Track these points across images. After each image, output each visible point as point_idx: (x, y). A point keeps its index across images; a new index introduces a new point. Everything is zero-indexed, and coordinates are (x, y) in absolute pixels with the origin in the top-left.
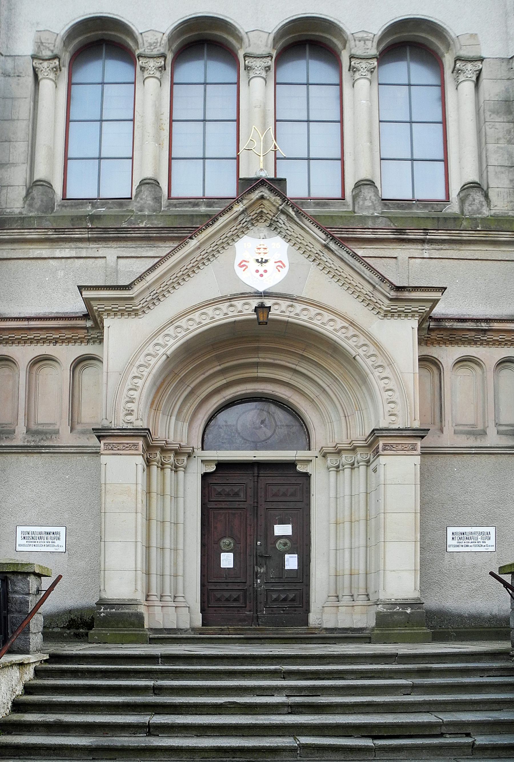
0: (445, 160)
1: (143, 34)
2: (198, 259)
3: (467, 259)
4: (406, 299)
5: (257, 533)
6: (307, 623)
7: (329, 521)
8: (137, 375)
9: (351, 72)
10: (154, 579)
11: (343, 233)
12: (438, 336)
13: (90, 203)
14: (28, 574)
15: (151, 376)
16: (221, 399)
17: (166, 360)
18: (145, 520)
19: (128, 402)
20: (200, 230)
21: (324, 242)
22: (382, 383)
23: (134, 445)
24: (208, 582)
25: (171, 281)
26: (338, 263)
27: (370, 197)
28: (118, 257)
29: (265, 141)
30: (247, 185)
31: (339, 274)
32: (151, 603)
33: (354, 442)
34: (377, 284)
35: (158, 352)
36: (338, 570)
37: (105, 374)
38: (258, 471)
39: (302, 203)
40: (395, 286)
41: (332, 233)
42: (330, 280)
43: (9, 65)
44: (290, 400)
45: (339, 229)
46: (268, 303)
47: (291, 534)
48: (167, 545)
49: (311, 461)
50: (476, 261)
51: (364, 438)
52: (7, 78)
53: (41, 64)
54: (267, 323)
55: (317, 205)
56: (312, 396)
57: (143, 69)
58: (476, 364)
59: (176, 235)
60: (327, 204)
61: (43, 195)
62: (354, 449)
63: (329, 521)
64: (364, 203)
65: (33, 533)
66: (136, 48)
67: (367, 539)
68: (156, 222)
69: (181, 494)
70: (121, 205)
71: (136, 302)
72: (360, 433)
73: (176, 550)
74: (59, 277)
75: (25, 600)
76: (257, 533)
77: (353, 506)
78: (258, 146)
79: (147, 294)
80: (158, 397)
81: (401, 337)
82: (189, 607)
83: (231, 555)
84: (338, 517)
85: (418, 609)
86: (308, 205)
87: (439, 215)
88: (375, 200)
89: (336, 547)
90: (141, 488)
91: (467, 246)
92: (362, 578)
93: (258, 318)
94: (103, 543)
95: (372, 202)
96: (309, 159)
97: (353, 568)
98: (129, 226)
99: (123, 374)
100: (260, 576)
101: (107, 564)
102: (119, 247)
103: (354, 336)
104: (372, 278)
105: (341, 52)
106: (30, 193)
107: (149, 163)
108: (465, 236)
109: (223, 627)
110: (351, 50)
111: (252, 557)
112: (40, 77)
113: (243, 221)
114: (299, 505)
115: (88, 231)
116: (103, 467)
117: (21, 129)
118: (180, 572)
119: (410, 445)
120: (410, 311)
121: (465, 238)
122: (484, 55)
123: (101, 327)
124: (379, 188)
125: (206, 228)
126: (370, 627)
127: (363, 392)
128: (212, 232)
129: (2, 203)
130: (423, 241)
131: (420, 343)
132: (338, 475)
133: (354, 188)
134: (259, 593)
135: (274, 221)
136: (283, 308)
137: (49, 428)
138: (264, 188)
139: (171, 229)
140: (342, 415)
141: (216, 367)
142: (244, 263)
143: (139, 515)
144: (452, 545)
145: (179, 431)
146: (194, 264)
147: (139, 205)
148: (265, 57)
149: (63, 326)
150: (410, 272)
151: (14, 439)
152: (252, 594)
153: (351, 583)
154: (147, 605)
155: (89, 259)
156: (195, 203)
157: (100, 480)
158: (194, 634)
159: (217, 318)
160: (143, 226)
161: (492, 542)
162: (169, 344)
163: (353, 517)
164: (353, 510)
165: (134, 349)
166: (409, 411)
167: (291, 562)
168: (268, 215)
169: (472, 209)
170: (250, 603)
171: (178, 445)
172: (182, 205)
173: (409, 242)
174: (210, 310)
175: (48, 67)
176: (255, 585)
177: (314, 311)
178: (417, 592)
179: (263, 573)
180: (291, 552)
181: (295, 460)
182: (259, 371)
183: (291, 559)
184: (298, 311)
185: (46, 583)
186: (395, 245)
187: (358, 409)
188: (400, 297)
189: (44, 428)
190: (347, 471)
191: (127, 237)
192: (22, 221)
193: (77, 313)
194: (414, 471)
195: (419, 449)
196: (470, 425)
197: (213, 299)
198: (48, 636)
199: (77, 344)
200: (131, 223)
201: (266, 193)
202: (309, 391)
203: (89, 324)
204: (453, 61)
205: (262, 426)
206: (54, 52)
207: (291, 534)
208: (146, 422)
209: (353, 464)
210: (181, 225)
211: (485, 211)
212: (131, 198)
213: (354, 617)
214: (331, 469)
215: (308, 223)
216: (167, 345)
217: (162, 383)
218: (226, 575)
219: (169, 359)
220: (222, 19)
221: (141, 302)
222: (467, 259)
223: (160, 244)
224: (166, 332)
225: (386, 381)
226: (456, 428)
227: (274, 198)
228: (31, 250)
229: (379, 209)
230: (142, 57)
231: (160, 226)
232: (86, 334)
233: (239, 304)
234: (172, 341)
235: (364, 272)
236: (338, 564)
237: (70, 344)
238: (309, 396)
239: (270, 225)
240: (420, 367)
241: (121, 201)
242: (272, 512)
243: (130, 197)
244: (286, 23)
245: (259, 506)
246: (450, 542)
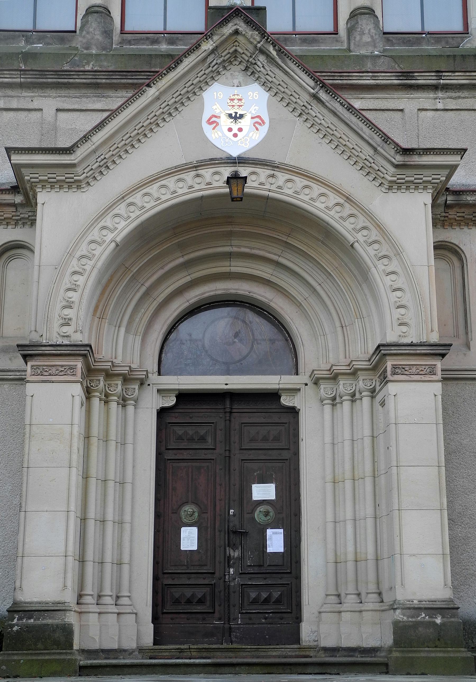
4: (415, 165)
5: (229, 498)
6: (297, 640)
7: (324, 478)
8: (77, 269)
10: (90, 568)
11: (336, 78)
12: (458, 214)
13: (23, 36)
15: (95, 271)
18: (80, 478)
19: (64, 307)
21: (312, 91)
22: (388, 280)
23: (72, 368)
26: (330, 119)
27: (369, 30)
31: (332, 132)
32: (84, 608)
33: (354, 363)
36: (338, 553)
37: (36, 268)
38: (231, 404)
39: (286, 40)
40: (401, 148)
41: (322, 78)
42: (321, 141)
44: (272, 304)
46: (244, 171)
47: (273, 497)
48: (110, 516)
49: (299, 390)
51: (367, 356)
54: (242, 198)
55: (304, 41)
56: (300, 298)
60: (316, 40)
62: (354, 373)
63: (324, 478)
64: (361, 39)
67: (376, 506)
68: (105, 64)
69: (130, 438)
70: (62, 40)
71: (79, 170)
72: (361, 350)
73: (121, 523)
76: (229, 498)
77: (356, 455)
79: (93, 159)
81: (408, 217)
82: (136, 614)
85: (451, 617)
86: (293, 43)
87: (457, 52)
88: (375, 34)
89: (335, 519)
92: (371, 565)
93: (231, 192)
94: (22, 514)
95: (372, 37)
97: (358, 551)
98: (73, 69)
100: (234, 563)
101: (26, 546)
102: (59, 97)
103: (351, 215)
109: (182, 647)
111: (222, 534)
113: (213, 64)
114: (285, 454)
115: (21, 75)
118: (126, 559)
119: (427, 367)
120: (421, 181)
123: (33, 204)
125: (168, 72)
126: (386, 646)
127: (364, 292)
128: (175, 78)
130: (435, 88)
131: (435, 225)
132: (335, 410)
133: (348, 19)
134: (231, 590)
135: (251, 63)
138: (239, 20)
139: (124, 73)
140: (338, 324)
142: (214, 119)
143: (74, 470)
147: (84, 41)
150: (420, 128)
152: (222, 593)
153: (357, 574)
154: (79, 610)
155: (20, 112)
156: (154, 39)
157: (23, 419)
158: (142, 659)
159: (180, 192)
162: (120, 227)
163: (356, 473)
165: (74, 231)
166: (424, 318)
167: (275, 541)
168: (243, 56)
170: (220, 605)
172: (137, 41)
173: (418, 89)
174: (171, 182)
176: (227, 577)
177: (300, 182)
179: (238, 558)
181: (279, 389)
182: (233, 264)
183: (274, 537)
184: (280, 183)
188: (408, 164)
190: (346, 405)
191: (69, 83)
193: (4, 184)
194: (434, 404)
195: (439, 372)
197: (176, 167)
201: (241, 26)
202: (295, 291)
203: (18, 199)
205: (236, 340)
207: (273, 497)
208: (86, 335)
209: (353, 395)
212: (75, 32)
216: (116, 229)
217: (110, 281)
218: (187, 562)
219: (118, 248)
223: (111, 93)
224: (116, 211)
225: (393, 277)
227: (251, 33)
229: (380, 45)
231: (110, 69)
232: (14, 213)
233: (207, 173)
234: (123, 223)
236: (338, 544)
238: (295, 298)
239: (246, 69)
241: (63, 35)
242: (249, 465)
243: (74, 30)
245: (232, 456)
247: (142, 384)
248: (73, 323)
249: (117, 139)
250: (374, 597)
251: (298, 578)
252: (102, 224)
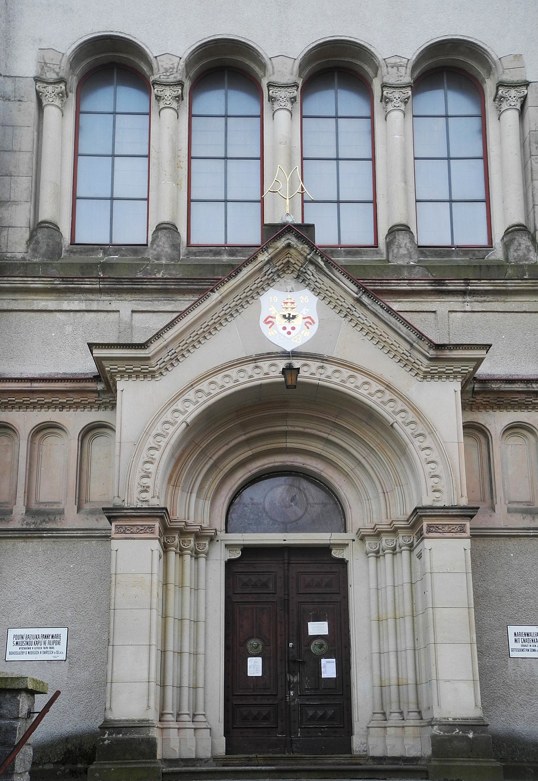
0: (487, 201)
1: (158, 58)
2: (220, 315)
3: (513, 312)
5: (289, 634)
7: (370, 617)
8: (153, 445)
9: (383, 103)
10: (170, 692)
12: (484, 399)
13: (101, 249)
14: (18, 691)
15: (169, 447)
16: (246, 473)
17: (186, 428)
18: (160, 617)
19: (143, 477)
20: (223, 282)
21: (356, 296)
22: (423, 454)
23: (151, 527)
24: (234, 695)
25: (191, 339)
26: (372, 319)
27: (406, 244)
28: (133, 312)
29: (291, 182)
30: (273, 232)
32: (166, 725)
33: (394, 523)
34: (415, 342)
35: (177, 419)
37: (118, 444)
39: (332, 252)
40: (434, 344)
41: (364, 285)
42: (364, 338)
43: (9, 87)
44: (323, 474)
45: (372, 279)
46: (297, 363)
47: (327, 633)
48: (186, 649)
49: (348, 545)
50: (524, 314)
52: (6, 103)
53: (44, 88)
55: (348, 253)
56: (346, 469)
57: (158, 98)
58: (528, 431)
59: (196, 287)
60: (359, 253)
61: (50, 239)
63: (370, 617)
64: (398, 251)
65: (28, 637)
66: (151, 74)
67: (415, 639)
68: (174, 272)
69: (202, 584)
71: (153, 362)
72: (401, 512)
73: (196, 654)
74: (67, 333)
75: (12, 727)
76: (289, 634)
77: (397, 598)
78: (284, 188)
79: (165, 353)
80: (177, 470)
81: (442, 402)
82: (210, 729)
83: (259, 660)
84: (381, 612)
85: (481, 733)
86: (338, 254)
88: (411, 248)
90: (157, 578)
91: (514, 297)
92: (411, 688)
93: (286, 380)
94: (110, 647)
95: (408, 250)
96: (338, 202)
97: (400, 677)
99: (138, 444)
100: (293, 687)
101: (114, 674)
102: (134, 300)
103: (391, 400)
104: (409, 336)
105: (372, 81)
106: (34, 237)
107: (167, 206)
108: (511, 285)
109: (250, 756)
110: (383, 77)
112: (45, 103)
113: (269, 272)
115: (99, 282)
116: (113, 553)
117: (23, 161)
118: (201, 684)
119: (458, 526)
120: (451, 371)
121: (510, 288)
122: (529, 79)
124: (415, 234)
125: (229, 280)
128: (235, 285)
129: (3, 246)
130: (464, 293)
131: (464, 408)
135: (302, 272)
137: (52, 508)
139: (191, 281)
140: (380, 490)
141: (240, 436)
142: (270, 319)
143: (154, 612)
145: (200, 511)
146: (216, 321)
147: (155, 253)
148: (290, 86)
149: (71, 388)
150: (451, 327)
151: (11, 520)
154: (161, 726)
155: (100, 313)
156: (216, 251)
157: (109, 569)
158: (216, 766)
159: (242, 380)
160: (160, 276)
162: (190, 410)
163: (397, 613)
164: (397, 604)
165: (150, 415)
167: (329, 669)
168: (295, 265)
169: (518, 255)
171: (199, 527)
172: (202, 253)
174: (233, 372)
175: (53, 92)
176: (288, 698)
177: (346, 373)
178: (480, 709)
179: (297, 682)
180: (328, 656)
181: (330, 544)
182: (288, 440)
183: (328, 665)
185: (40, 701)
186: (433, 297)
187: (398, 485)
188: (440, 358)
189: (47, 507)
190: (389, 557)
191: (143, 289)
192: (24, 268)
193: (87, 374)
194: (464, 557)
195: (468, 530)
196: (526, 502)
197: (237, 360)
199: (86, 410)
200: (146, 273)
201: (293, 241)
203: (100, 386)
204: (495, 86)
205: (292, 504)
206: (60, 74)
207: (327, 633)
208: (163, 499)
209: (394, 549)
210: (200, 276)
211: (532, 257)
212: (147, 245)
213: (406, 742)
214: (370, 555)
215: (338, 274)
216: (186, 411)
217: (184, 451)
218: (254, 686)
219: (189, 427)
220: (244, 43)
221: (158, 363)
222: (513, 312)
223: (179, 297)
224: (186, 397)
225: (428, 452)
226: (510, 506)
227: (302, 246)
228: (35, 302)
229: (415, 257)
230: (157, 84)
231: (178, 277)
233: (265, 365)
234: (192, 407)
235: (400, 329)
236: (383, 671)
237: (79, 410)
239: (298, 277)
240: (465, 435)
241: (136, 249)
244: (313, 48)
246: (512, 645)
248: (151, 490)
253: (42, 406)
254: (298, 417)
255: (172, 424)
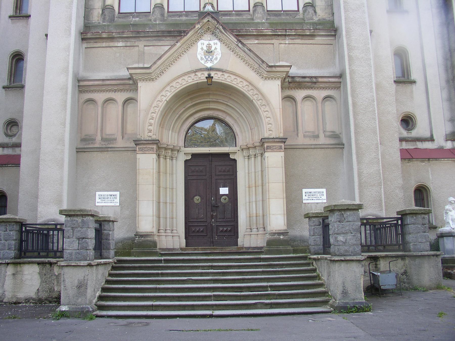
7: (245, 186)
15: (160, 112)
19: (149, 126)
23: (153, 148)
37: (139, 111)
55: (237, 15)
56: (236, 118)
63: (245, 186)
65: (104, 195)
69: (174, 172)
71: (153, 74)
79: (158, 70)
81: (272, 89)
103: (252, 89)
116: (138, 160)
118: (175, 216)
136: (219, 76)
140: (249, 128)
143: (155, 186)
144: (306, 199)
159: (189, 81)
161: (325, 197)
162: (168, 95)
165: (152, 97)
172: (174, 16)
174: (186, 78)
177: (233, 77)
184: (226, 78)
190: (253, 159)
198: (116, 254)
201: (210, 19)
203: (131, 82)
209: (255, 155)
217: (165, 113)
224: (166, 89)
225: (267, 113)
233: (199, 74)
234: (169, 94)
239: (213, 33)
242: (219, 181)
246: (304, 197)
247: (178, 151)
248: (152, 131)
249: (167, 62)
250: (262, 229)
251: (237, 222)
252: (161, 94)
253: (107, 91)
254: (214, 95)
255: (161, 102)
